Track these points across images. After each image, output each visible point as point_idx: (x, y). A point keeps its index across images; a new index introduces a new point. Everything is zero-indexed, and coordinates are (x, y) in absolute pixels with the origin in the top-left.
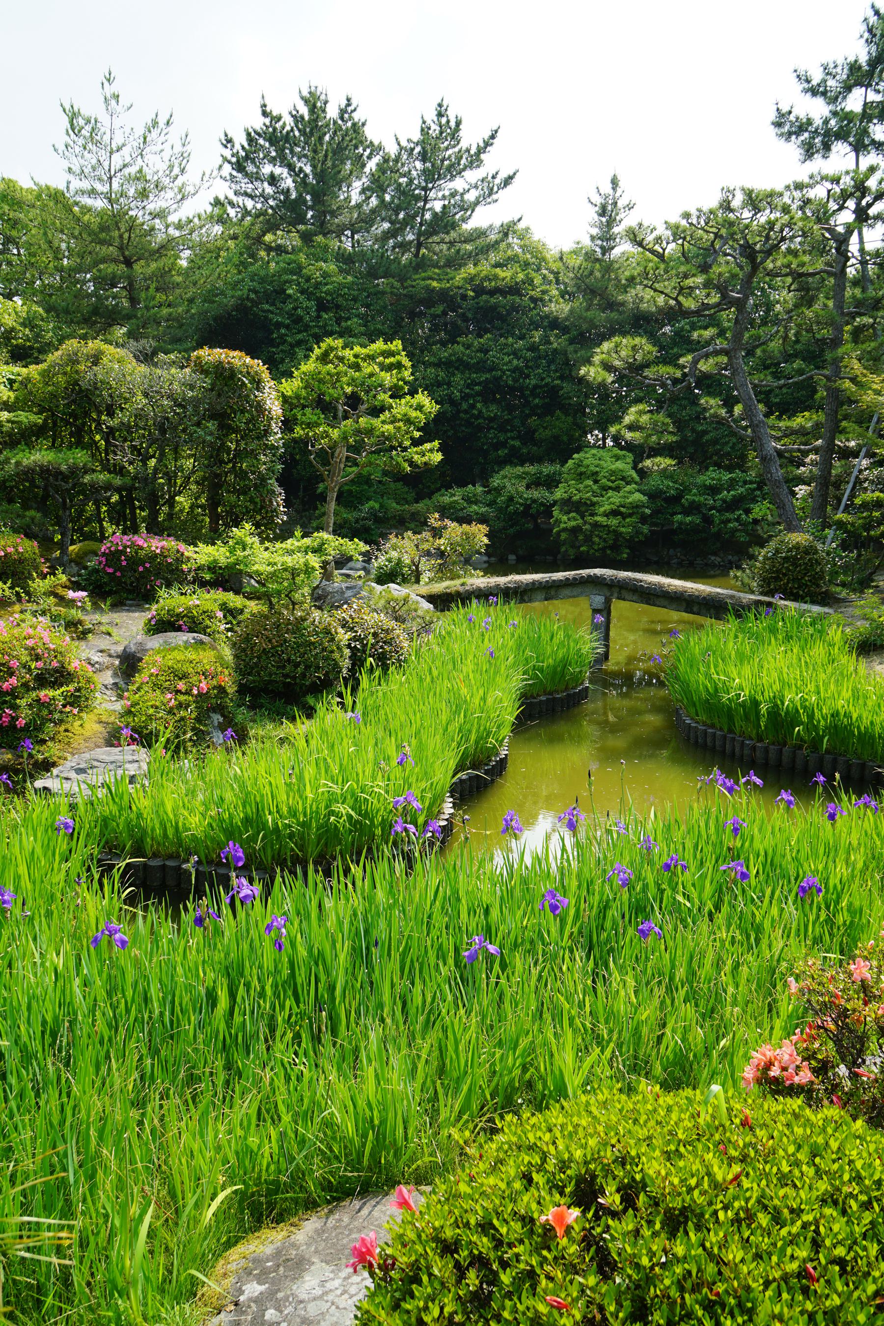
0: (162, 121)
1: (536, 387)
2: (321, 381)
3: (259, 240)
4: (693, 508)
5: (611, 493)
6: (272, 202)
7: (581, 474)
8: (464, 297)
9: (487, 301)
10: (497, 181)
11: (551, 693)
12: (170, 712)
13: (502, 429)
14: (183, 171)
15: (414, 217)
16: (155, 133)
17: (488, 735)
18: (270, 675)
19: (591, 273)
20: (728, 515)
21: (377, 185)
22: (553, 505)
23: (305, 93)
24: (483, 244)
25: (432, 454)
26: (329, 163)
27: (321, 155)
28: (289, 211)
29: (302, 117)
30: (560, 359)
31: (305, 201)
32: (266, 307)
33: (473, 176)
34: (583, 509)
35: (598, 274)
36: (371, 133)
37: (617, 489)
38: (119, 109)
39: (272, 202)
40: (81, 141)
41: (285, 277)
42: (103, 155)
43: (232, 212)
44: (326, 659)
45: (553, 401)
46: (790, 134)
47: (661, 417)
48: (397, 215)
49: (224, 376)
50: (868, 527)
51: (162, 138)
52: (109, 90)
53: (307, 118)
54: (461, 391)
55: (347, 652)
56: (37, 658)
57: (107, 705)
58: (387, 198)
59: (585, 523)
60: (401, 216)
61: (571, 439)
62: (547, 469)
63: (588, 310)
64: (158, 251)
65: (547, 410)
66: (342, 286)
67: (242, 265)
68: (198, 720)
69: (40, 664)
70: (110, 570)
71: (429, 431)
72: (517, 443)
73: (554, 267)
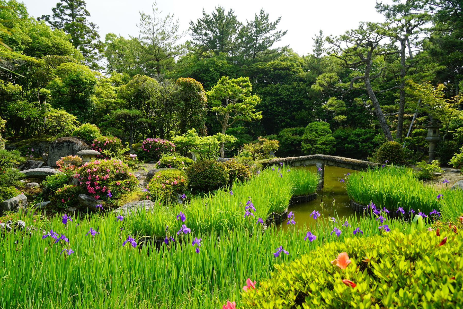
0: (171, 16)
1: (295, 101)
2: (220, 90)
3: (201, 54)
4: (352, 142)
5: (322, 137)
6: (205, 42)
7: (311, 130)
8: (270, 71)
9: (277, 72)
10: (281, 33)
11: (303, 195)
12: (163, 190)
13: (283, 116)
14: (176, 30)
15: (253, 46)
16: (168, 20)
17: (280, 203)
18: (200, 181)
19: (314, 62)
20: (364, 144)
21: (241, 35)
22: (302, 141)
23: (217, 8)
24: (276, 54)
25: (259, 116)
26: (225, 28)
27: (222, 26)
28: (212, 44)
29: (216, 15)
30: (303, 91)
31: (217, 41)
32: (203, 75)
33: (272, 32)
34: (312, 142)
35: (316, 62)
36: (239, 19)
37: (324, 135)
38: (157, 13)
39: (205, 42)
40: (145, 22)
41: (209, 65)
42: (151, 27)
43: (192, 45)
44: (220, 177)
45: (301, 106)
46: (381, 11)
47: (341, 101)
48: (247, 45)
49: (188, 86)
50: (418, 141)
51: (171, 21)
52: (155, 7)
53: (217, 15)
54: (269, 103)
55: (228, 175)
56: (117, 169)
57: (140, 190)
58: (244, 40)
59: (313, 147)
60: (248, 46)
61: (307, 118)
62: (299, 129)
63: (313, 74)
64: (167, 56)
65: (299, 109)
66: (228, 68)
67: (195, 62)
68: (173, 194)
69: (118, 171)
70: (146, 150)
71: (258, 108)
72: (289, 120)
73: (301, 61)
